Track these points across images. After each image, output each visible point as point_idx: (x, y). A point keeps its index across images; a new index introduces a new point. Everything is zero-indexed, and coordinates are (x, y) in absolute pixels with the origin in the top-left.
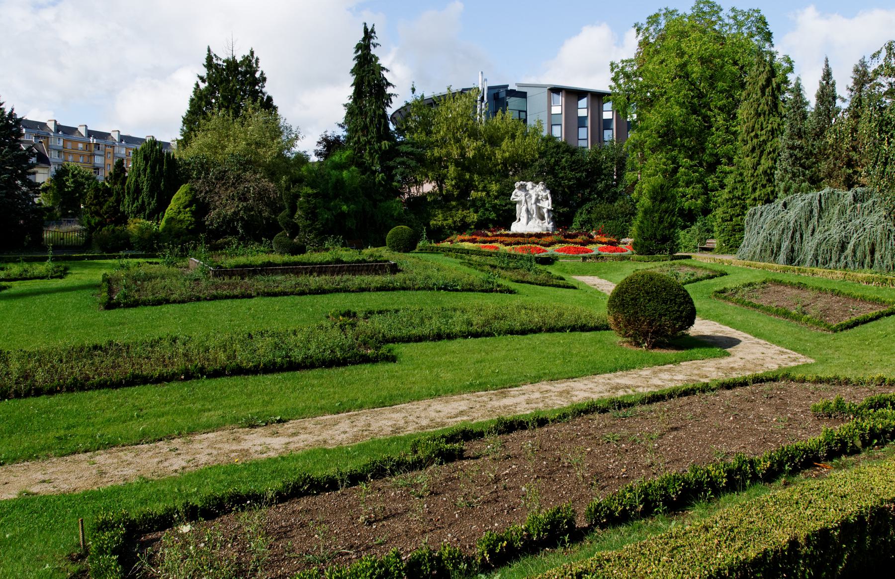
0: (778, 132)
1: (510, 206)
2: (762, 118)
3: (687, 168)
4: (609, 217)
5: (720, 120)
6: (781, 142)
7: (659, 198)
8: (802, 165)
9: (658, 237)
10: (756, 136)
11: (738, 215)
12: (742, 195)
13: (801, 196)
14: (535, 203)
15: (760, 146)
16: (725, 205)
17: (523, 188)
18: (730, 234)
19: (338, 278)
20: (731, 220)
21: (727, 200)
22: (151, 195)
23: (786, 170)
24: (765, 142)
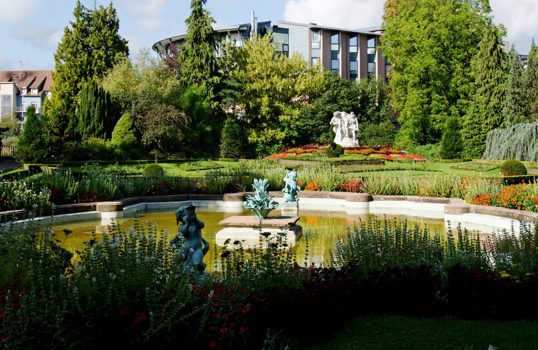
0: (501, 80)
1: (308, 127)
2: (491, 70)
3: (438, 101)
4: (378, 135)
5: (459, 67)
6: (507, 86)
7: (454, 127)
8: (520, 105)
9: (455, 149)
10: (487, 82)
11: (477, 135)
12: (479, 122)
13: (522, 125)
14: (347, 126)
15: (490, 89)
16: (467, 127)
17: (339, 116)
18: (471, 147)
19: (378, 166)
20: (472, 138)
21: (469, 124)
22: (99, 121)
23: (511, 108)
24: (493, 87)
